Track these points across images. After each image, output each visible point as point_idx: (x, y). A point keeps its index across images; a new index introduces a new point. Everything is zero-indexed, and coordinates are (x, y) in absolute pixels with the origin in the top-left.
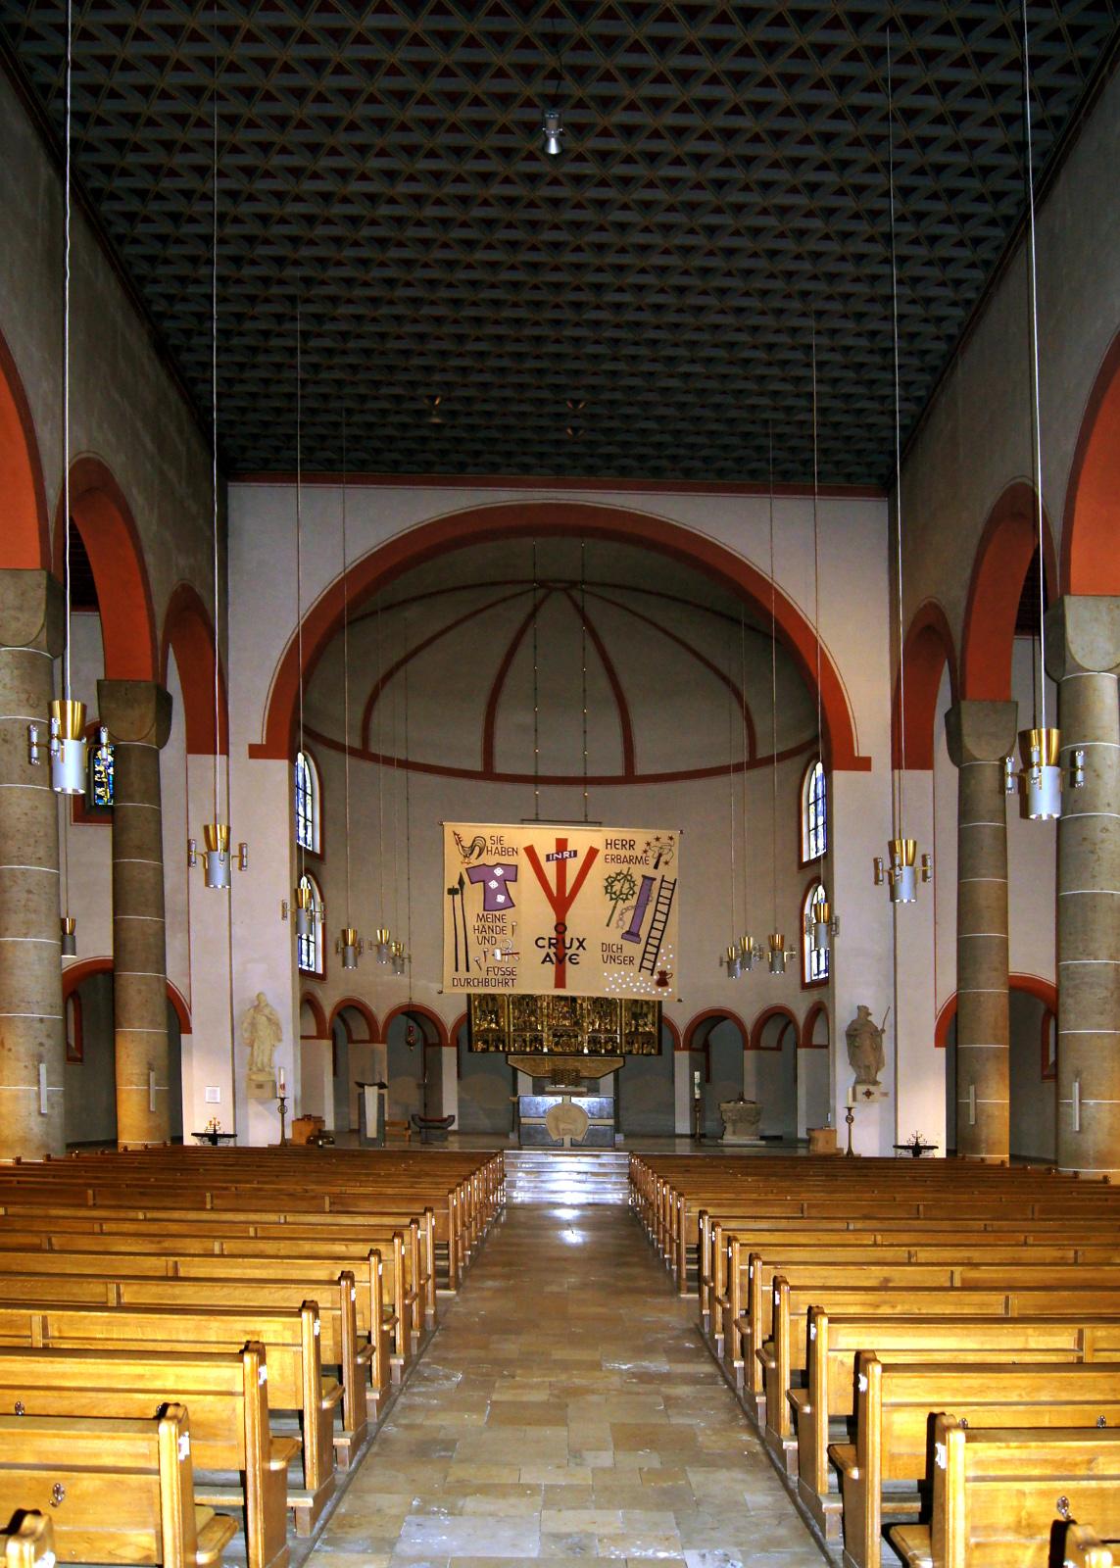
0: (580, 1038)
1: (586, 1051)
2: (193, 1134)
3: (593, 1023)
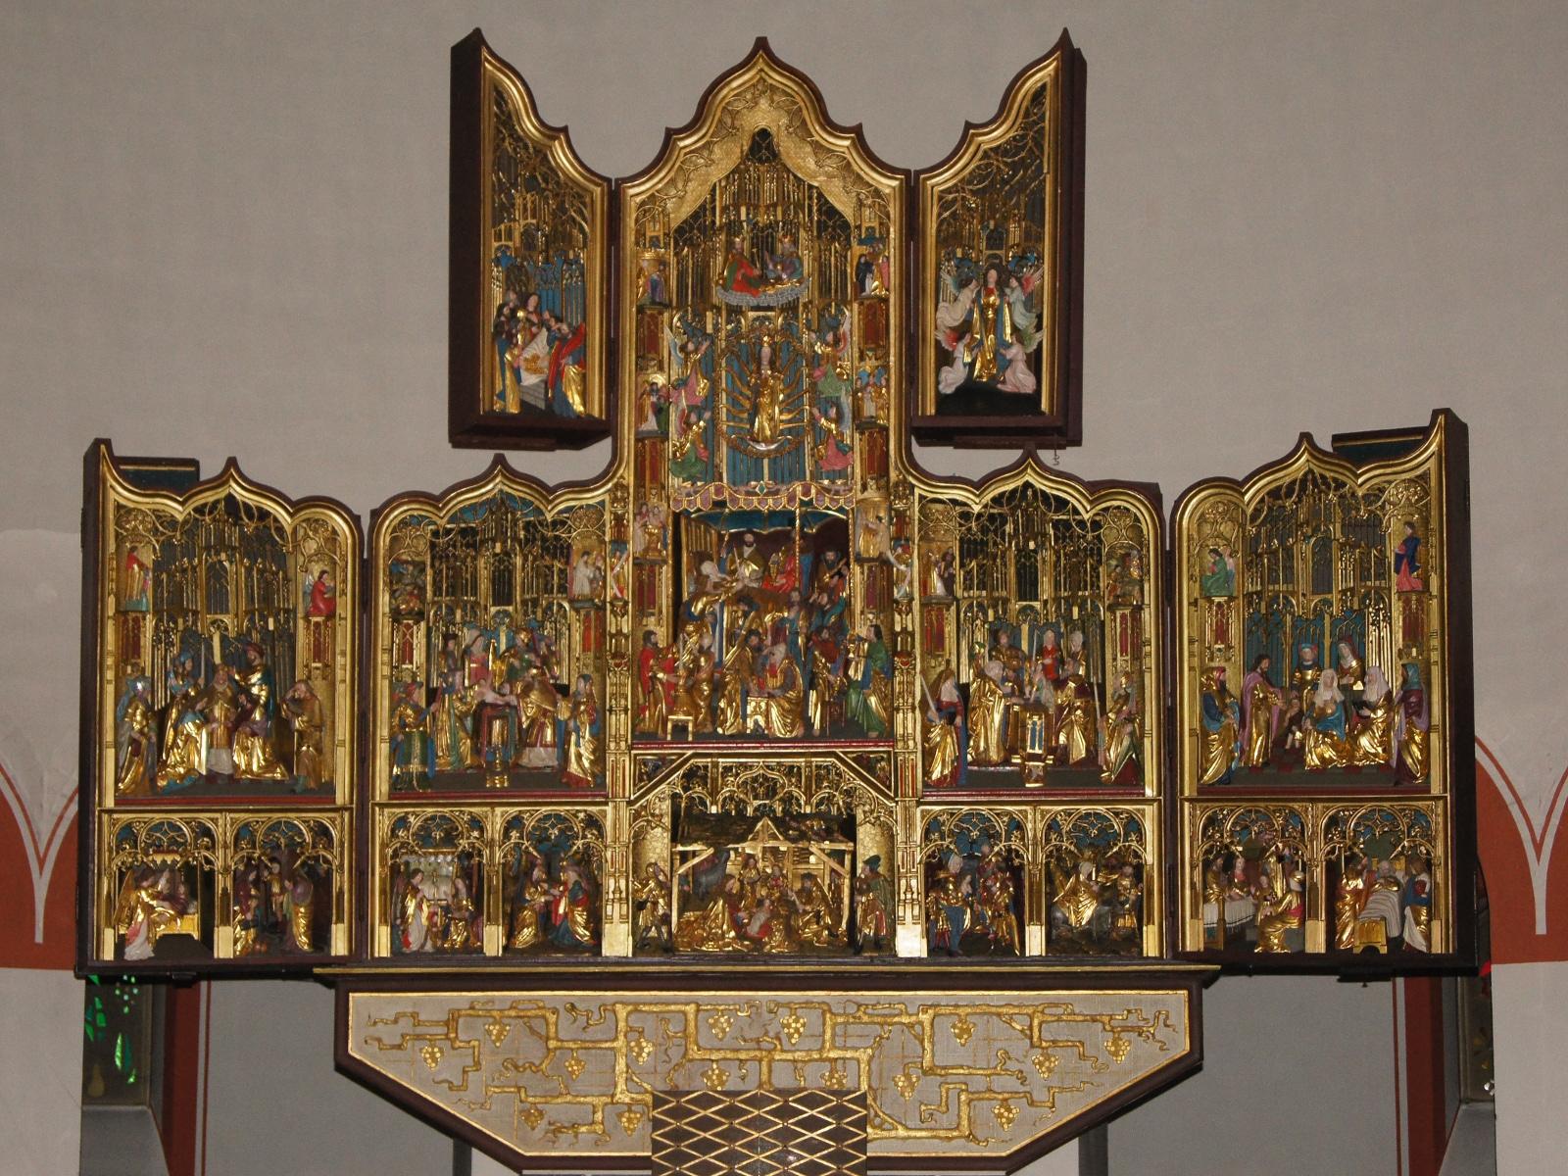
0: (868, 841)
1: (911, 942)
2: (1072, 64)
3: (959, 713)
